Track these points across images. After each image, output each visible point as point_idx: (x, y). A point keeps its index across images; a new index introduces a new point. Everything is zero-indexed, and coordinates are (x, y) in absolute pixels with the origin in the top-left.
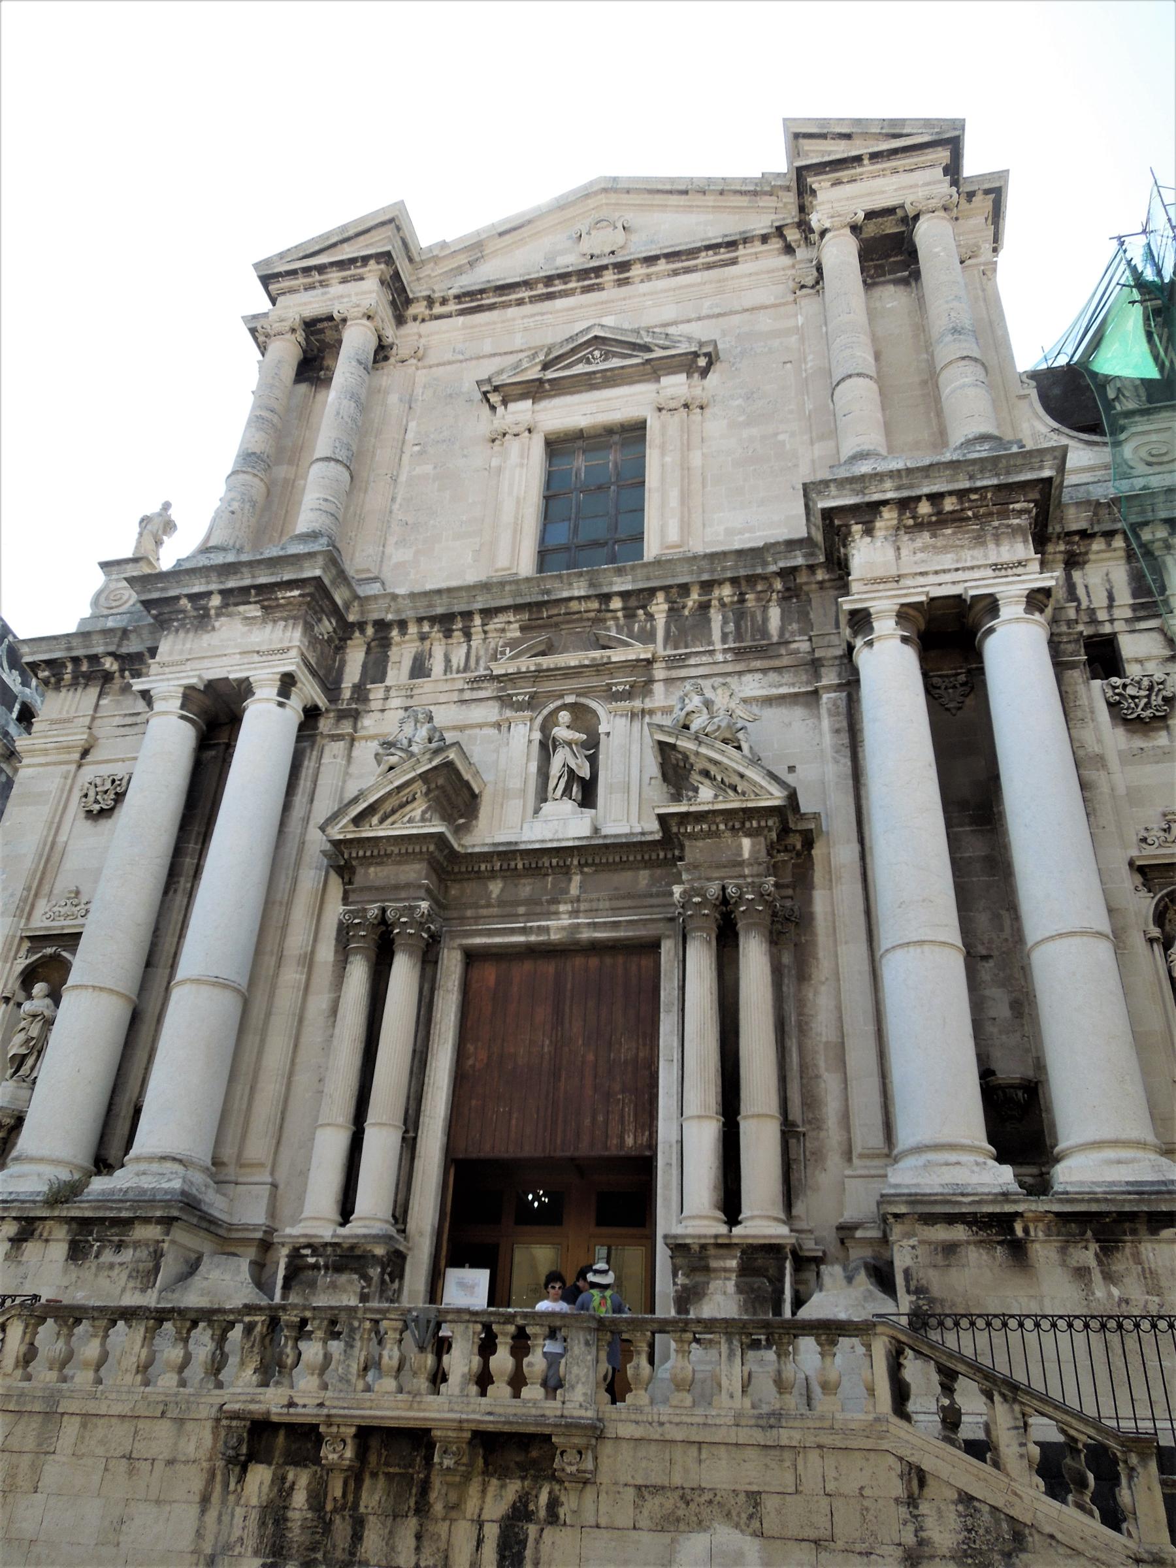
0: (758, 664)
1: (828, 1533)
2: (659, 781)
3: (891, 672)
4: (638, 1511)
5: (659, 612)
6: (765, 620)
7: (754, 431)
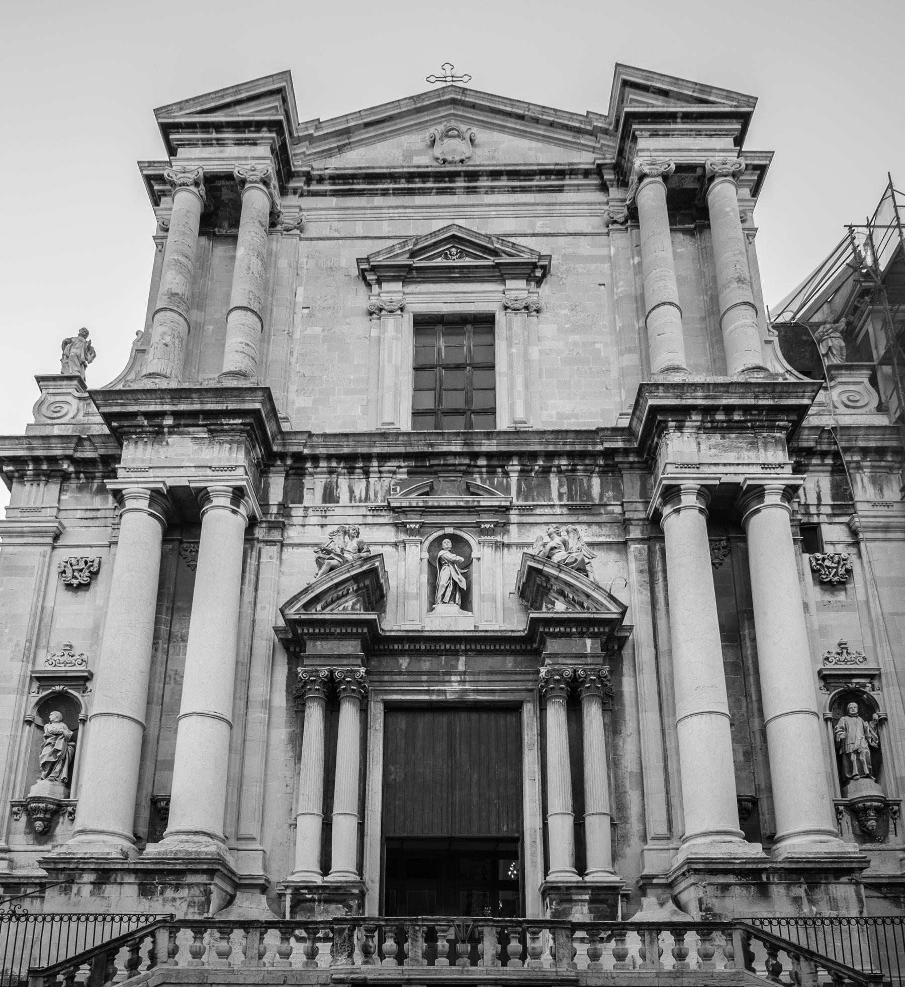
0: (584, 518)
2: (515, 597)
5: (514, 471)
6: (590, 486)
7: (577, 338)
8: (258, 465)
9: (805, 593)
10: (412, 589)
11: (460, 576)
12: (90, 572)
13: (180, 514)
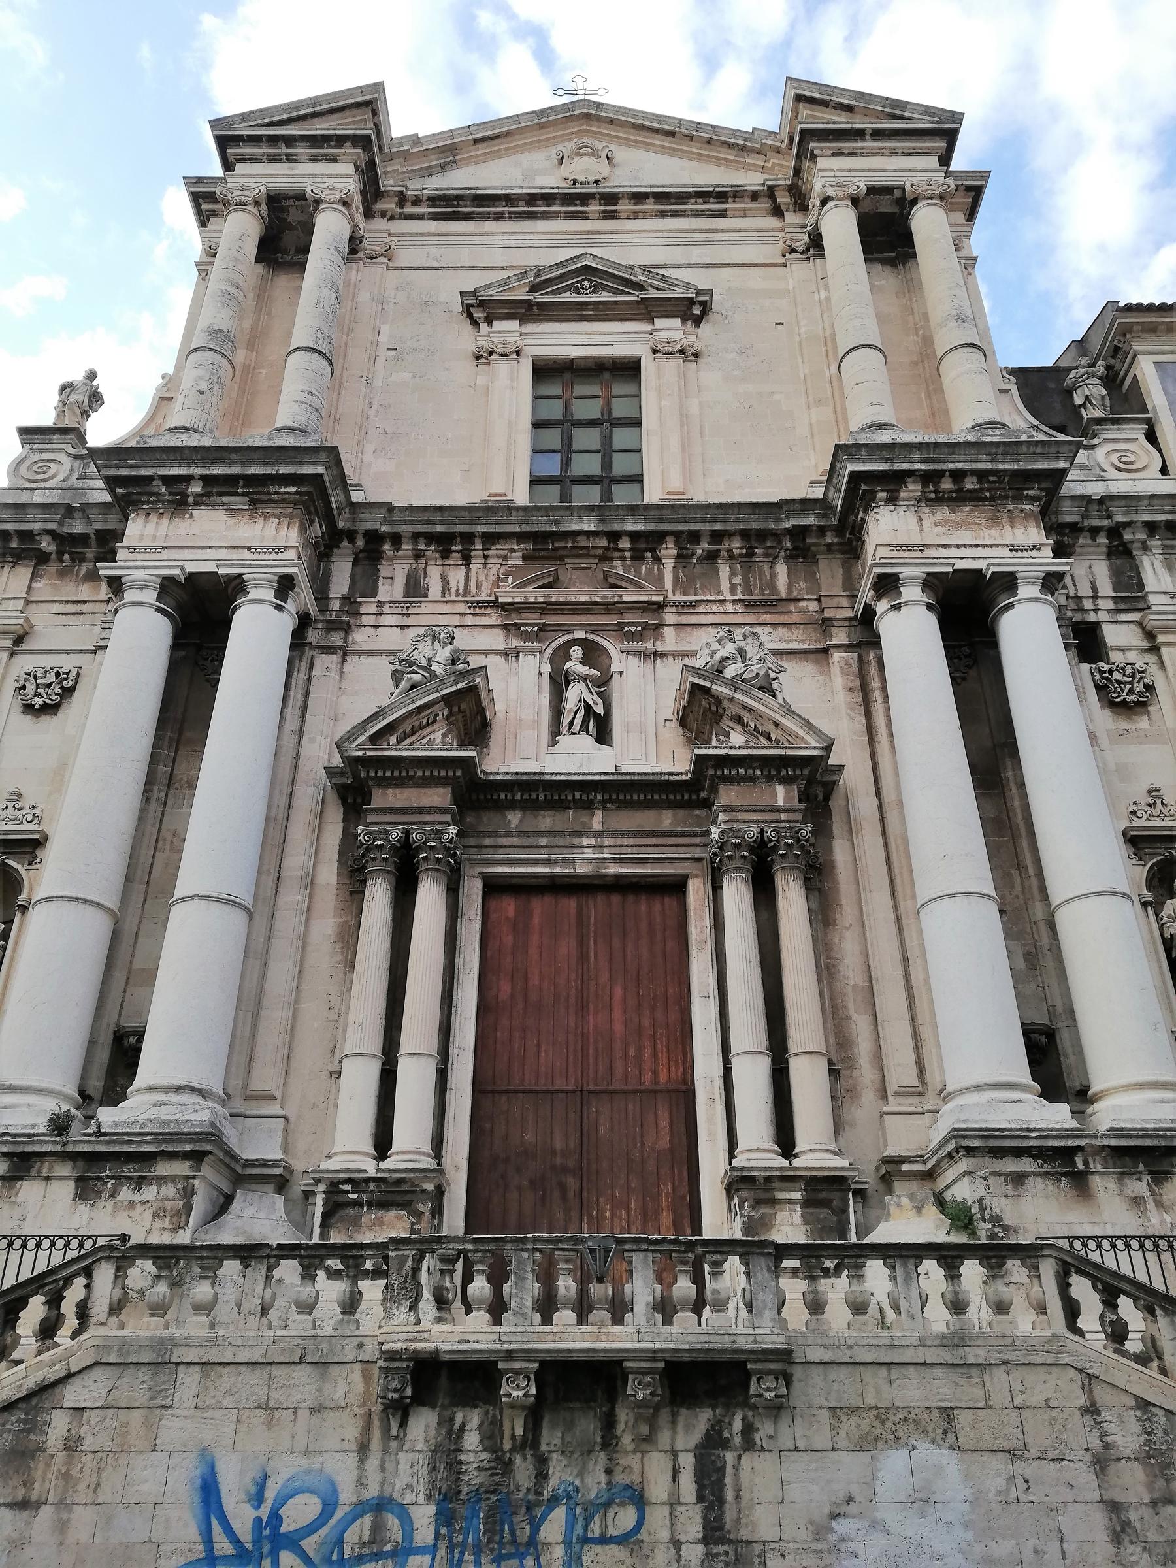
0: (767, 618)
1: (1021, 1443)
2: (674, 725)
3: (912, 637)
4: (835, 1432)
5: (668, 557)
6: (773, 576)
8: (316, 546)
9: (1089, 719)
10: (527, 715)
11: (596, 697)
12: (62, 688)
13: (200, 614)
